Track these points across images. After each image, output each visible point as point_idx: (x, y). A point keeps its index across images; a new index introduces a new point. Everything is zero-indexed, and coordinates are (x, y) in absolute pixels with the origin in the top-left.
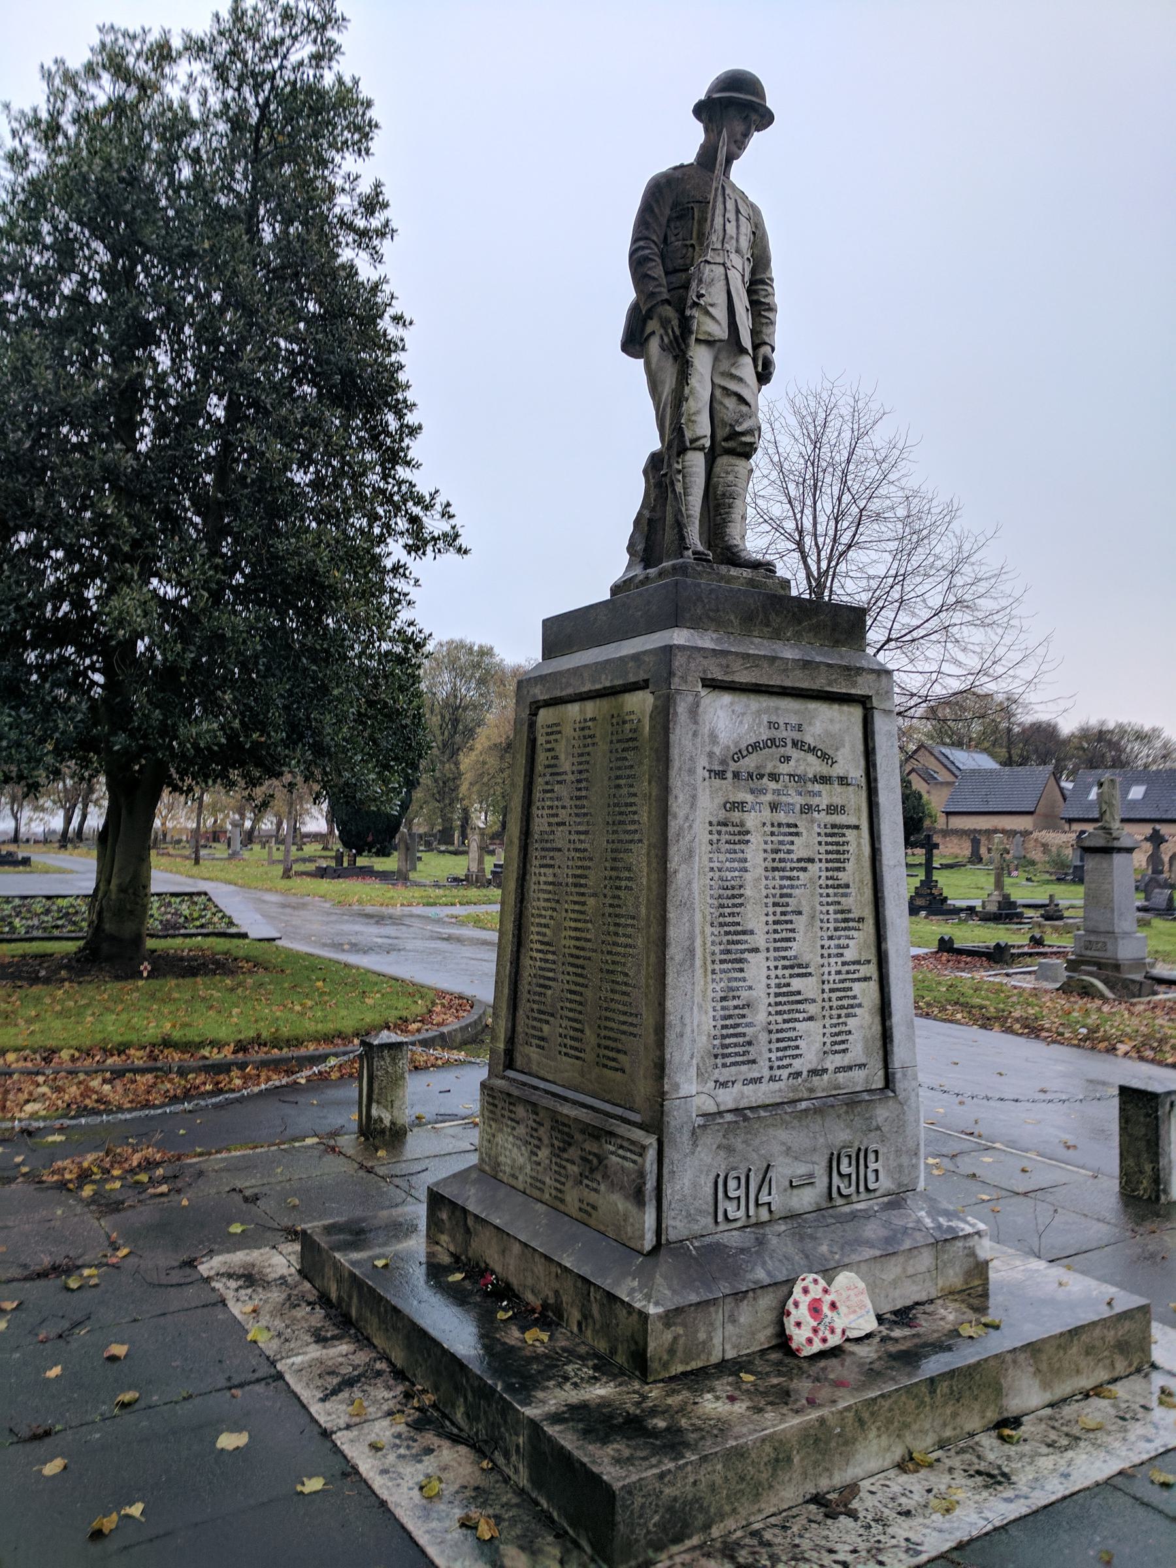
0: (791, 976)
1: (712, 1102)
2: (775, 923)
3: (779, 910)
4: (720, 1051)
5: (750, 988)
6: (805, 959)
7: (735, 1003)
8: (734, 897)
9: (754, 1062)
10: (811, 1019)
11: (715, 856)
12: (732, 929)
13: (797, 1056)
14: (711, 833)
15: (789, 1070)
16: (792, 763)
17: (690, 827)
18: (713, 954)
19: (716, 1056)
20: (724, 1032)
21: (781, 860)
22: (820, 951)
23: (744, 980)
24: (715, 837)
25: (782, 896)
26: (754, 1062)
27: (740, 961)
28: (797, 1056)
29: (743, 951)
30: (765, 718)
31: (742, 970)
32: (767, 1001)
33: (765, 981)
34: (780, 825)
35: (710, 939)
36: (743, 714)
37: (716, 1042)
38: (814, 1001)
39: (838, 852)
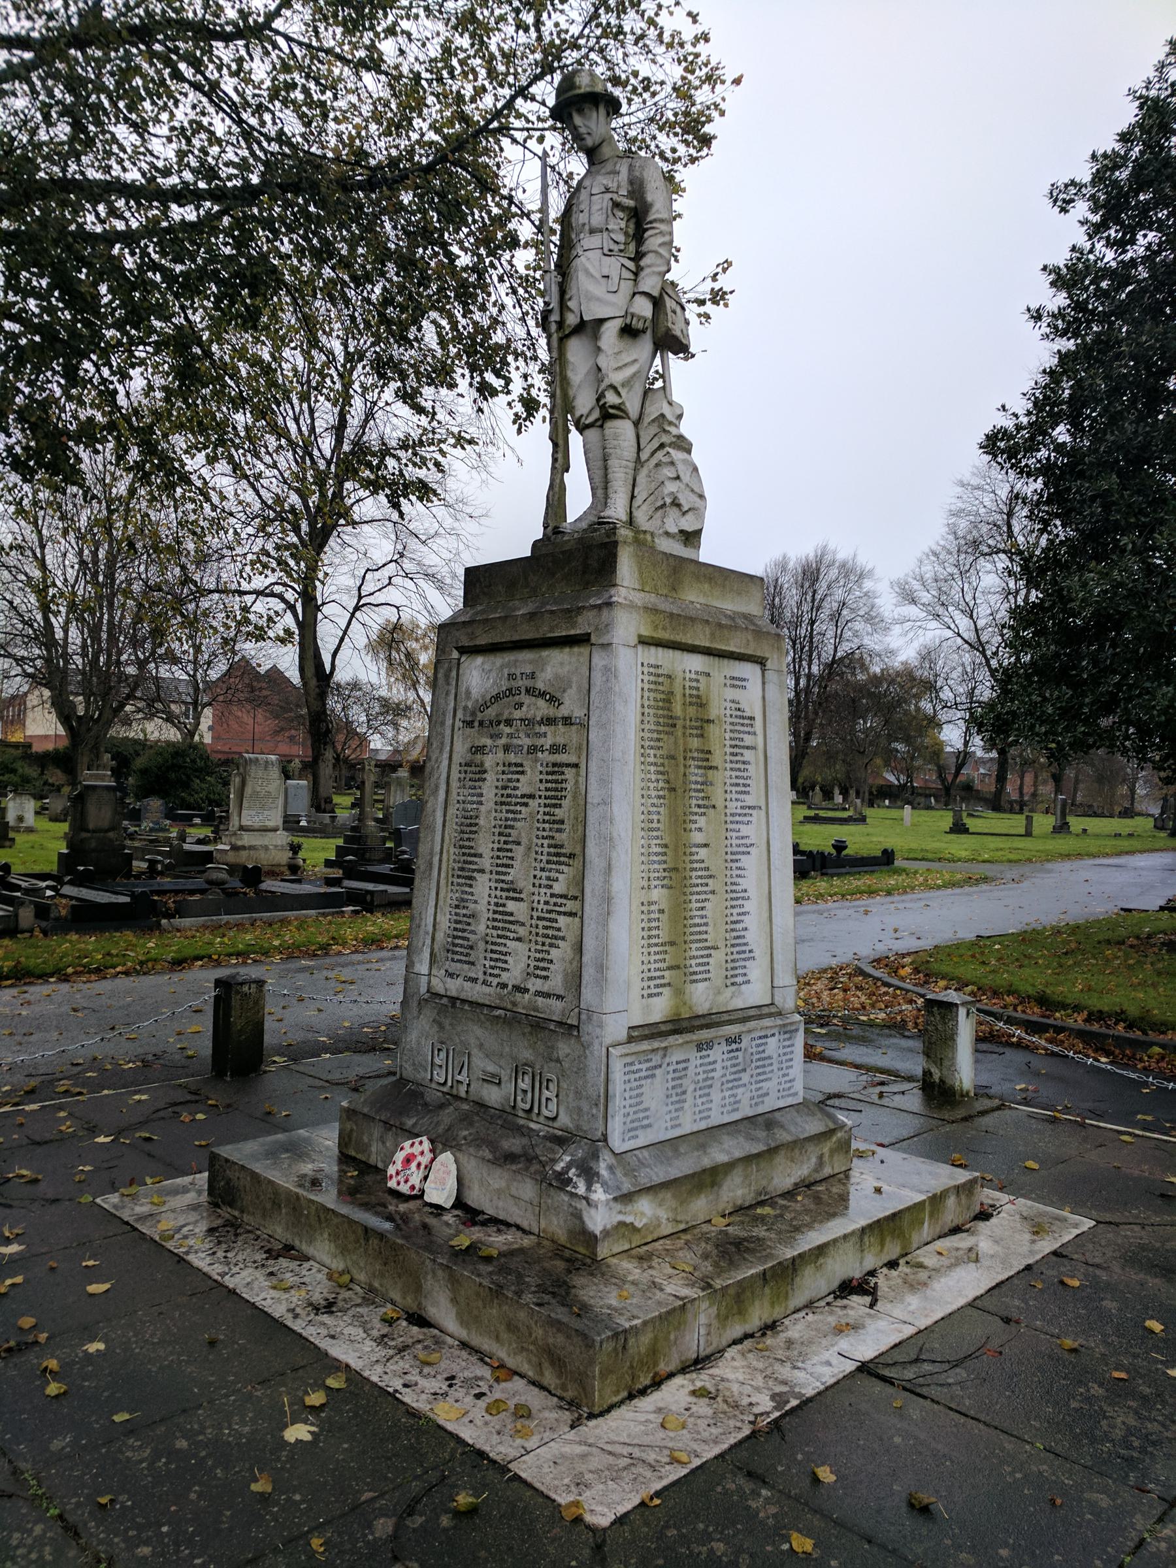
9: (473, 964)
10: (519, 939)
16: (524, 708)
27: (471, 878)
30: (506, 671)
38: (523, 924)
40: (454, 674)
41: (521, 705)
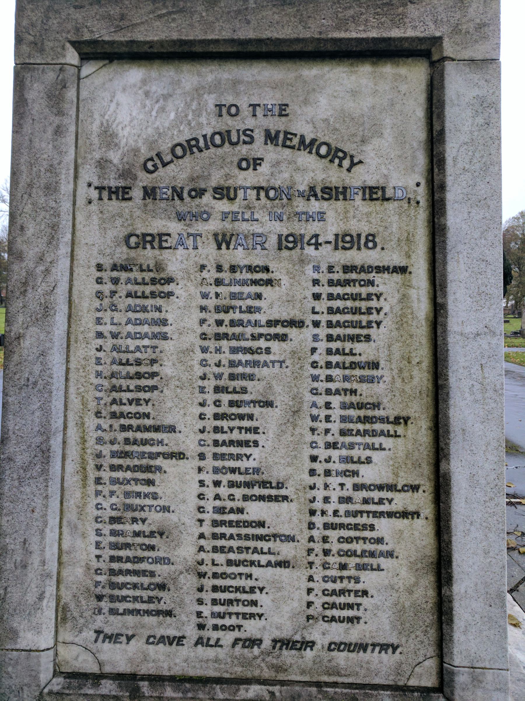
0: (245, 498)
1: (90, 658)
2: (216, 417)
3: (226, 398)
4: (107, 591)
5: (166, 509)
6: (275, 475)
7: (137, 527)
8: (139, 376)
9: (169, 613)
10: (283, 564)
11: (107, 316)
12: (134, 422)
13: (252, 616)
14: (99, 281)
15: (237, 634)
16: (264, 168)
17: (47, 271)
18: (99, 455)
19: (99, 598)
20: (115, 566)
21: (233, 323)
22: (308, 465)
23: (155, 496)
24: (107, 288)
25: (232, 377)
26: (169, 613)
27: (148, 469)
28: (252, 616)
29: (153, 456)
30: (211, 100)
31: (150, 482)
32: (197, 531)
33: (193, 502)
34: (233, 269)
35: (92, 435)
36: (166, 97)
37: (101, 578)
38: (291, 539)
39: (356, 311)
40: (71, 94)
41: (257, 162)
